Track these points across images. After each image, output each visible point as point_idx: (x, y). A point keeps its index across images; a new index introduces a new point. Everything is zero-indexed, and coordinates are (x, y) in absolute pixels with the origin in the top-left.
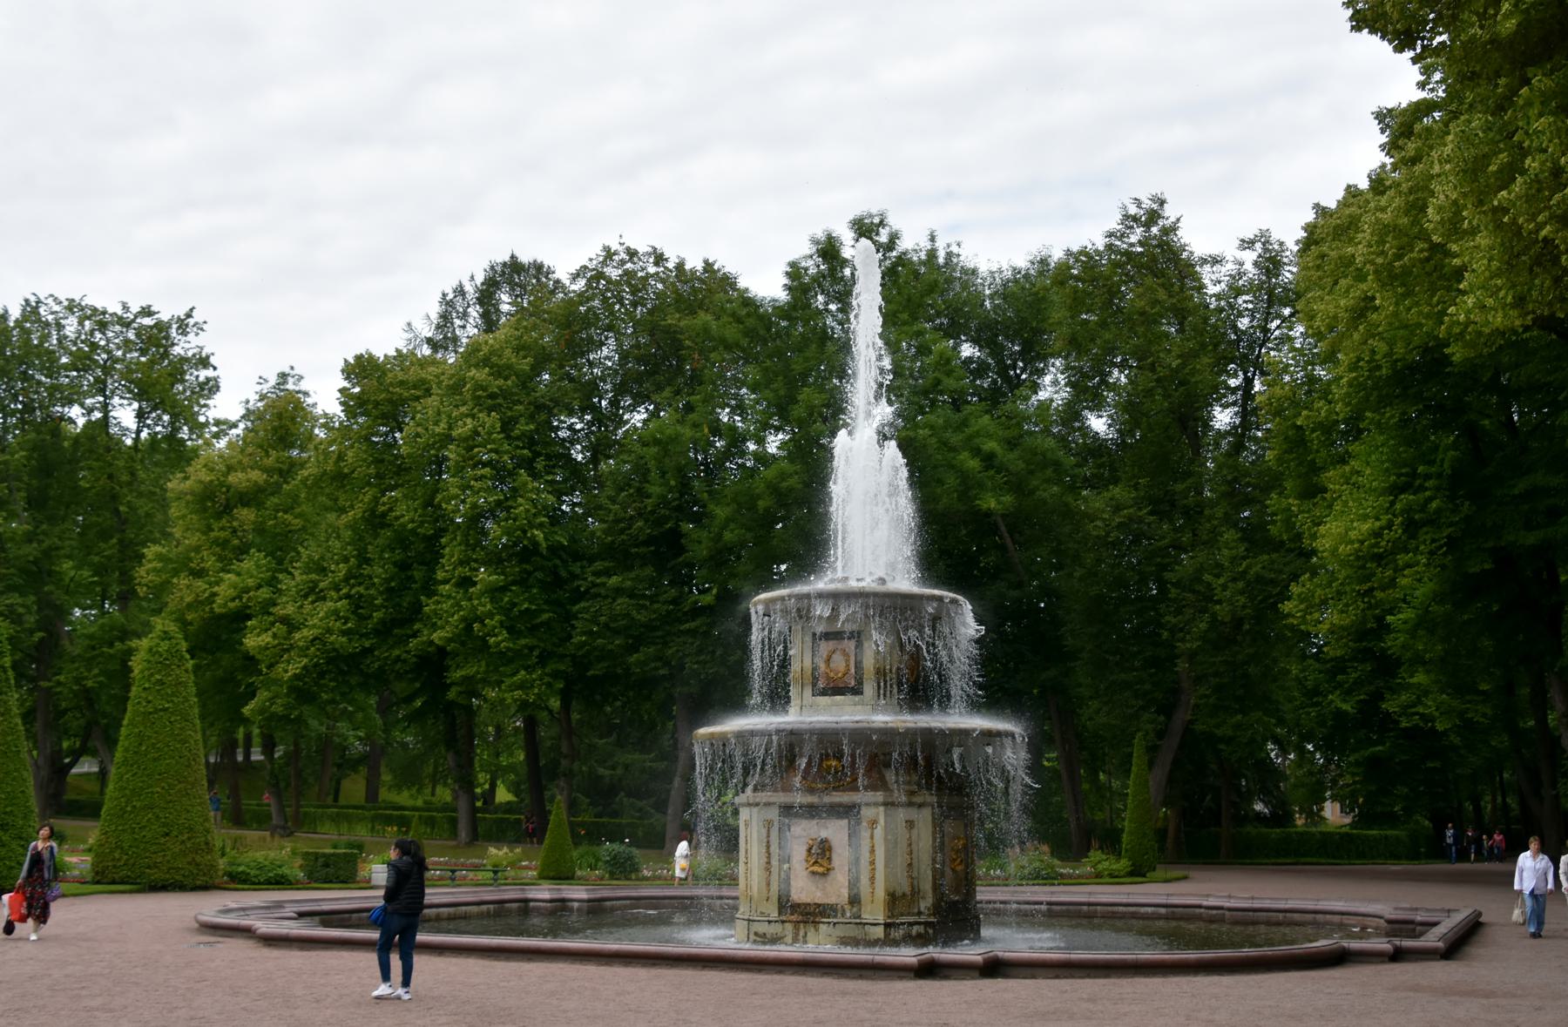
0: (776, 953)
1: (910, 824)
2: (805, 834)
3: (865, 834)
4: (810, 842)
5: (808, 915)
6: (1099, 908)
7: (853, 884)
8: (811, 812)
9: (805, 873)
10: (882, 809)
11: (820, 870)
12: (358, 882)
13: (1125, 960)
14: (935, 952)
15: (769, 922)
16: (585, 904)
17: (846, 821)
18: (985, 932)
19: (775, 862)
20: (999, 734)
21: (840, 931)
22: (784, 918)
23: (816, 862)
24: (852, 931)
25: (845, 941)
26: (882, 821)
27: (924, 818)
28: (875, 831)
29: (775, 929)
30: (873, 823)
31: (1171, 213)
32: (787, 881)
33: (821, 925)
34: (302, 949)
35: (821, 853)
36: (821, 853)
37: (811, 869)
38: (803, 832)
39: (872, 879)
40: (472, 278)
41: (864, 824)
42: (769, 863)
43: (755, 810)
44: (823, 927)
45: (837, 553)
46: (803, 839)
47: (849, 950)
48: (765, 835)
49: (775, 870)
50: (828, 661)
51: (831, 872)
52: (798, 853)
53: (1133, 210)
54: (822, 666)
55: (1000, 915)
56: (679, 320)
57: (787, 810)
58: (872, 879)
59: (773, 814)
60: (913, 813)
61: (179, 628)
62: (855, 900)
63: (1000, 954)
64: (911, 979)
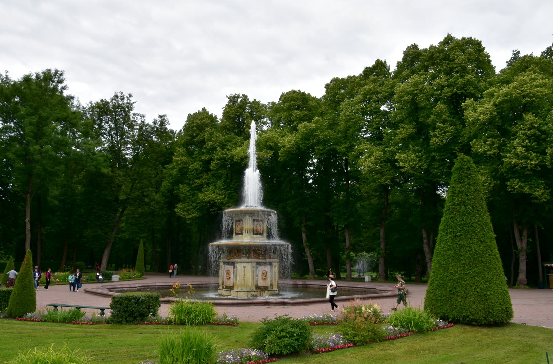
3: (274, 269)
5: (261, 289)
7: (271, 281)
12: (113, 282)
19: (255, 276)
21: (270, 292)
24: (272, 292)
25: (216, 295)
29: (255, 293)
30: (275, 267)
31: (132, 100)
32: (257, 281)
34: (237, 306)
35: (265, 274)
36: (265, 274)
38: (261, 269)
39: (275, 280)
44: (266, 292)
47: (119, 293)
49: (255, 278)
50: (256, 227)
52: (260, 274)
53: (119, 95)
54: (255, 228)
56: (78, 177)
57: (258, 264)
58: (275, 280)
59: (254, 264)
61: (478, 153)
62: (271, 285)
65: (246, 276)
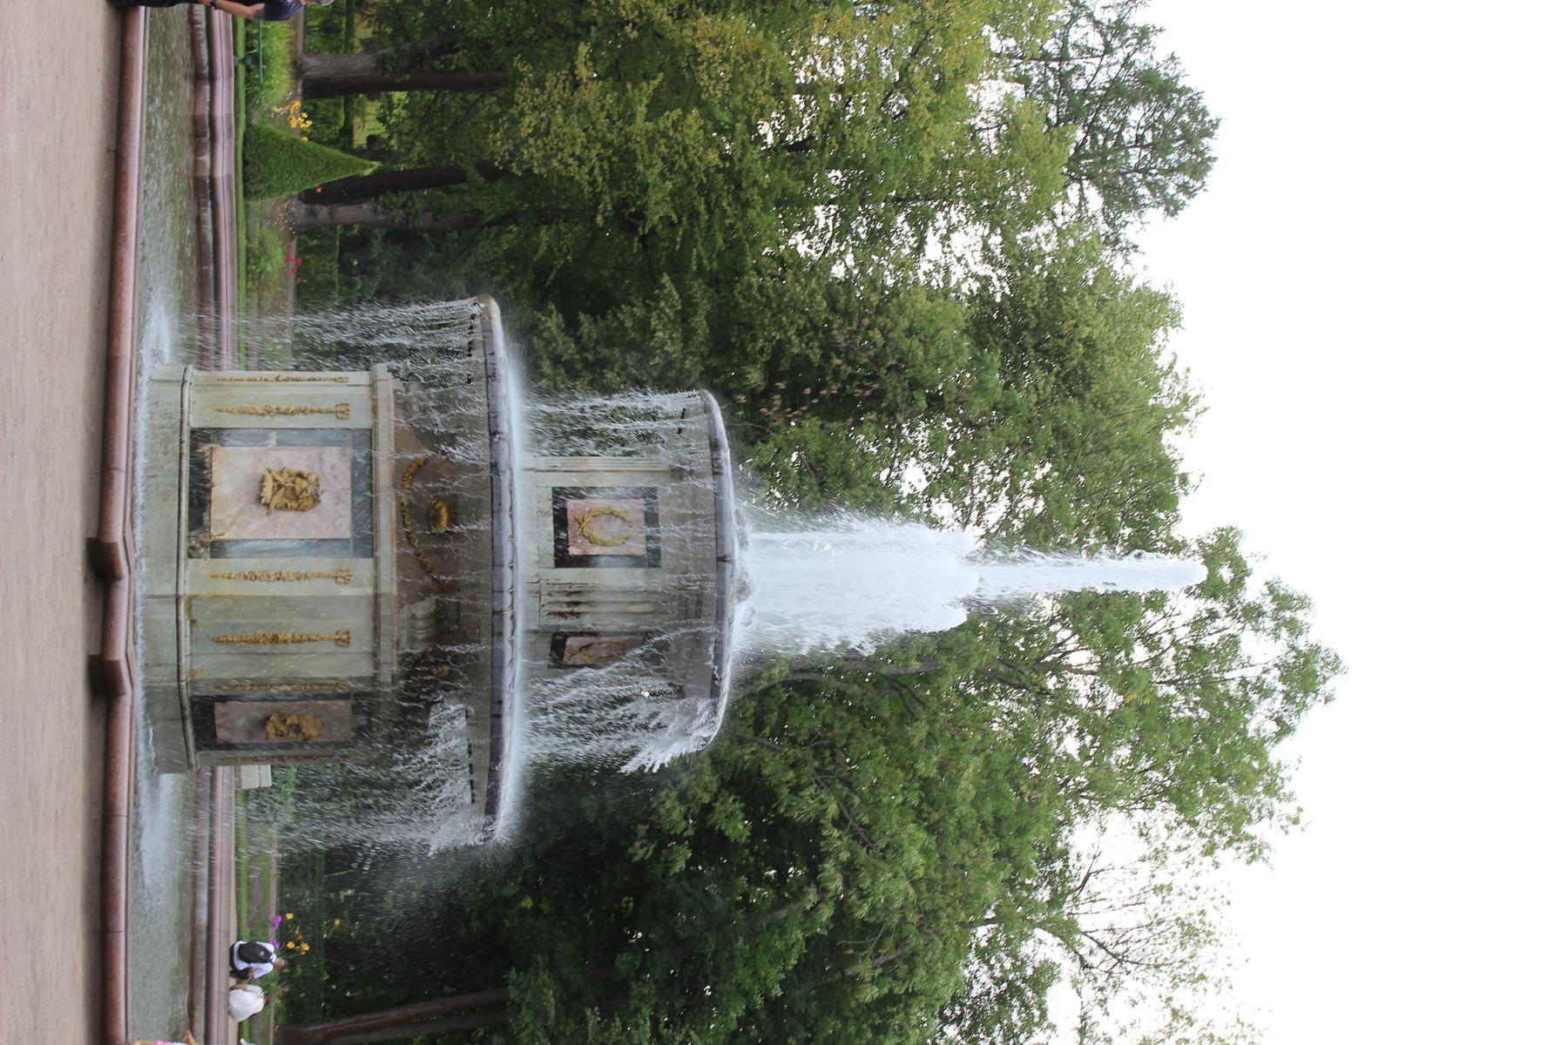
0: (122, 927)
1: (343, 640)
2: (327, 469)
3: (326, 564)
4: (313, 478)
6: (212, 268)
8: (364, 475)
9: (261, 470)
10: (370, 591)
11: (268, 491)
13: (116, 910)
14: (132, 700)
16: (207, 174)
17: (348, 535)
18: (168, 781)
20: (491, 808)
23: (280, 486)
26: (346, 591)
27: (349, 666)
37: (269, 477)
40: (1271, 826)
42: (279, 412)
43: (366, 391)
46: (316, 469)
48: (325, 407)
49: (268, 422)
51: (264, 510)
52: (295, 459)
55: (197, 803)
60: (361, 642)
63: (124, 583)
64: (87, 530)
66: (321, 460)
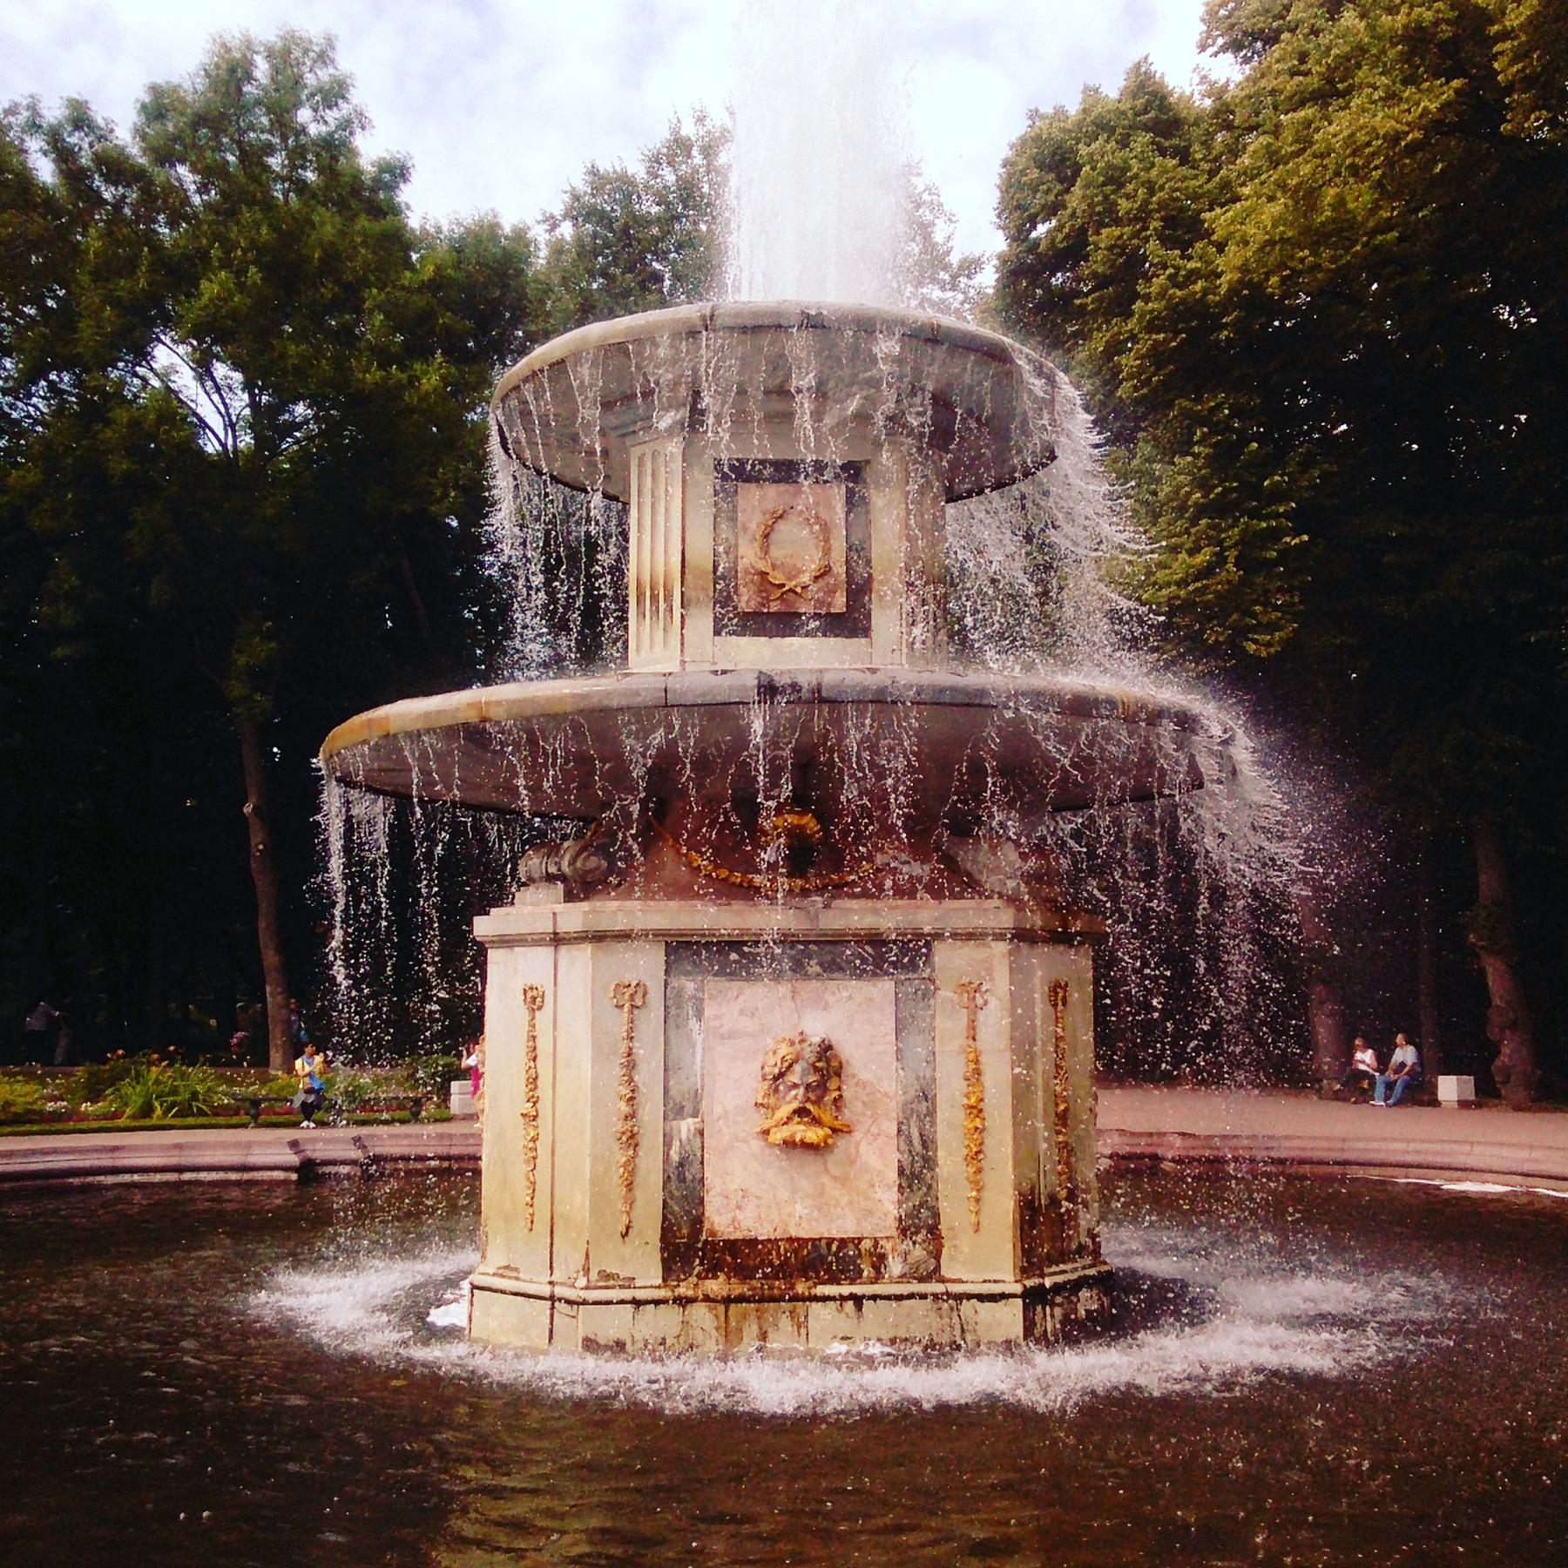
15: (637, 1303)
22: (684, 1290)
23: (801, 1112)
28: (981, 1015)
33: (816, 1307)
41: (945, 994)
45: (730, 274)
51: (842, 1142)
53: (689, 130)
59: (647, 964)
65: (545, 1107)
66: (731, 1035)
